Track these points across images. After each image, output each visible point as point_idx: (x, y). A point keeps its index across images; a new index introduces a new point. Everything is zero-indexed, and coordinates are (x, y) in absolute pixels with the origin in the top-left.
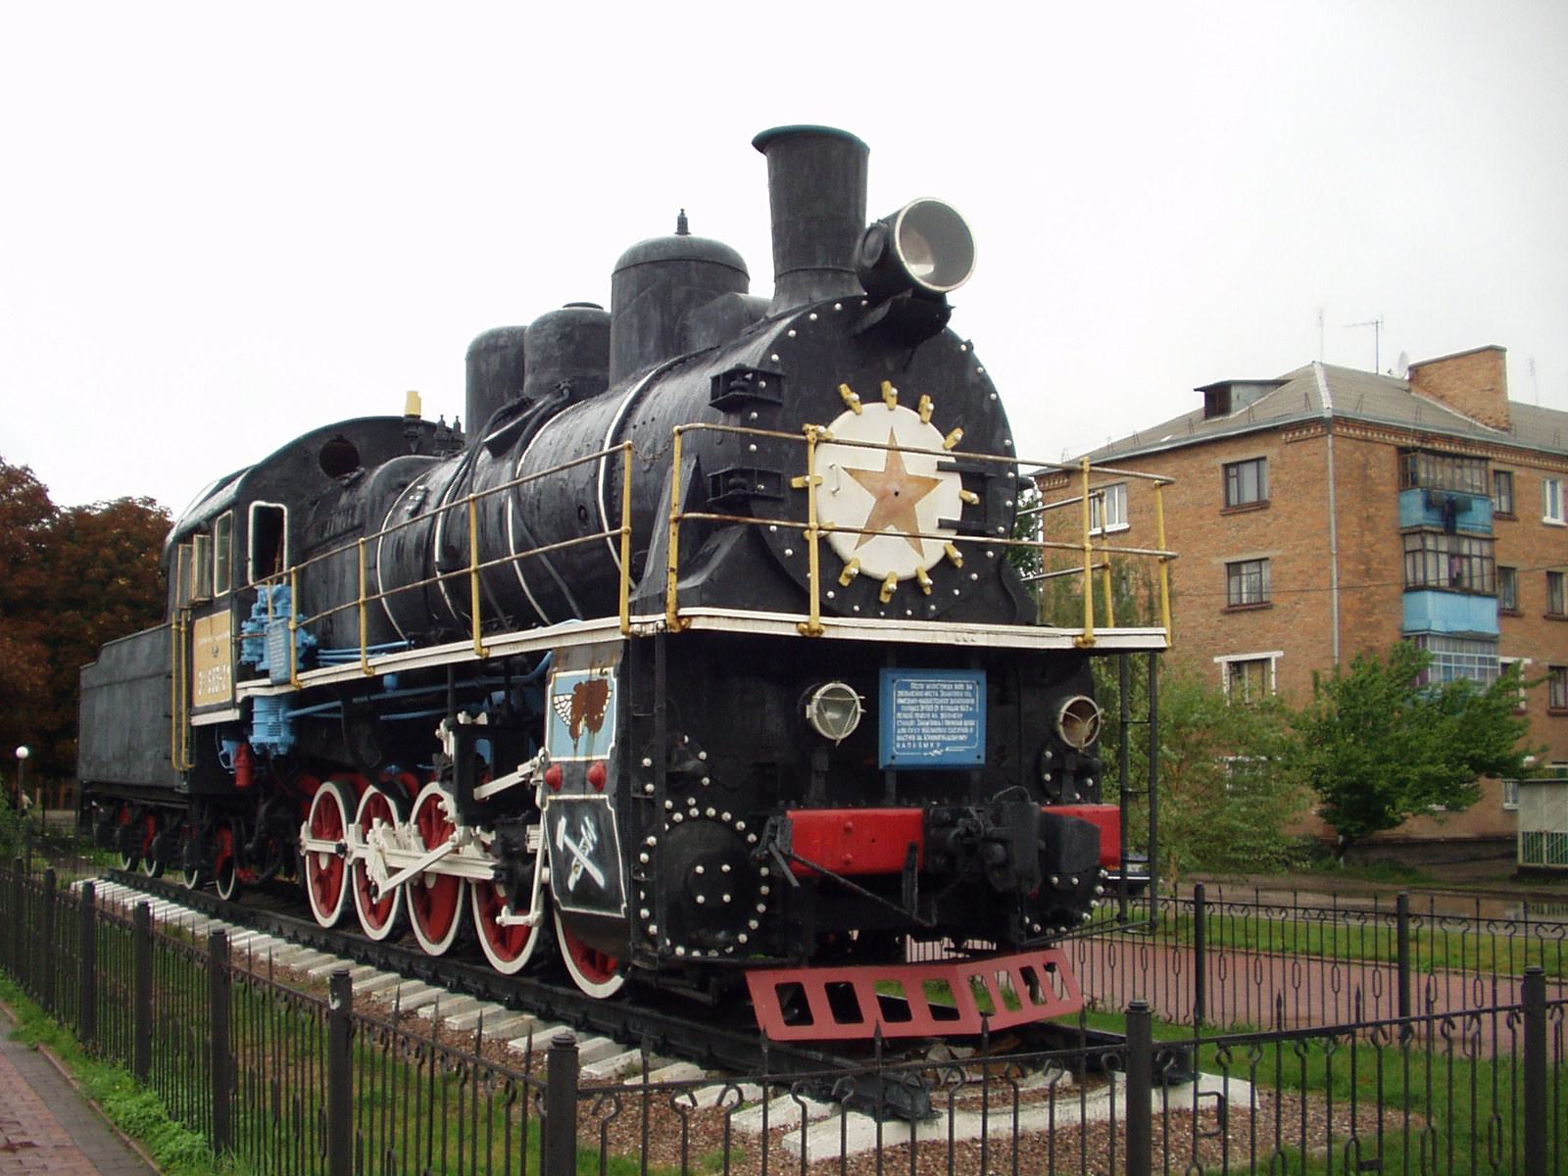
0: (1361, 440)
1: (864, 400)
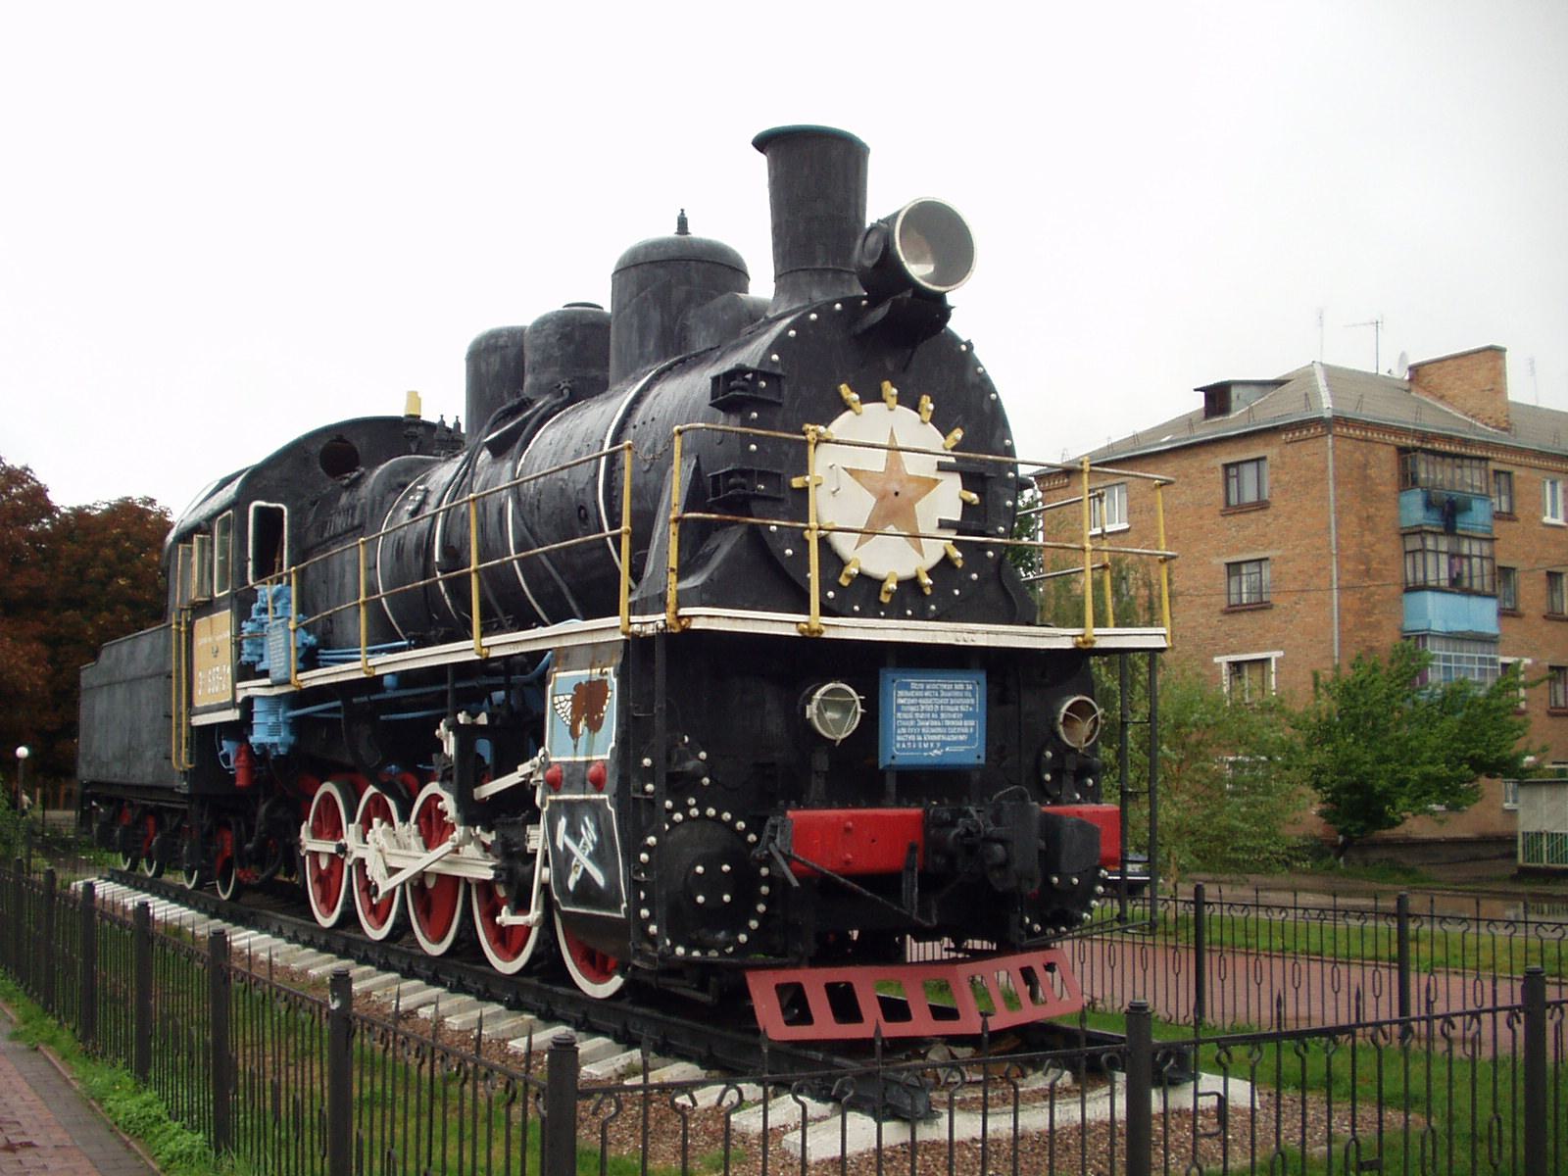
0: (1361, 440)
1: (864, 400)
